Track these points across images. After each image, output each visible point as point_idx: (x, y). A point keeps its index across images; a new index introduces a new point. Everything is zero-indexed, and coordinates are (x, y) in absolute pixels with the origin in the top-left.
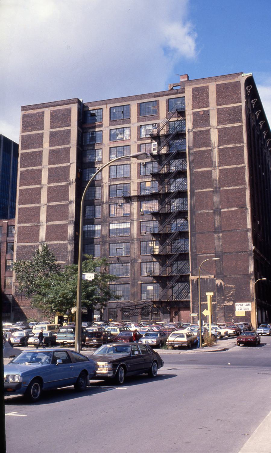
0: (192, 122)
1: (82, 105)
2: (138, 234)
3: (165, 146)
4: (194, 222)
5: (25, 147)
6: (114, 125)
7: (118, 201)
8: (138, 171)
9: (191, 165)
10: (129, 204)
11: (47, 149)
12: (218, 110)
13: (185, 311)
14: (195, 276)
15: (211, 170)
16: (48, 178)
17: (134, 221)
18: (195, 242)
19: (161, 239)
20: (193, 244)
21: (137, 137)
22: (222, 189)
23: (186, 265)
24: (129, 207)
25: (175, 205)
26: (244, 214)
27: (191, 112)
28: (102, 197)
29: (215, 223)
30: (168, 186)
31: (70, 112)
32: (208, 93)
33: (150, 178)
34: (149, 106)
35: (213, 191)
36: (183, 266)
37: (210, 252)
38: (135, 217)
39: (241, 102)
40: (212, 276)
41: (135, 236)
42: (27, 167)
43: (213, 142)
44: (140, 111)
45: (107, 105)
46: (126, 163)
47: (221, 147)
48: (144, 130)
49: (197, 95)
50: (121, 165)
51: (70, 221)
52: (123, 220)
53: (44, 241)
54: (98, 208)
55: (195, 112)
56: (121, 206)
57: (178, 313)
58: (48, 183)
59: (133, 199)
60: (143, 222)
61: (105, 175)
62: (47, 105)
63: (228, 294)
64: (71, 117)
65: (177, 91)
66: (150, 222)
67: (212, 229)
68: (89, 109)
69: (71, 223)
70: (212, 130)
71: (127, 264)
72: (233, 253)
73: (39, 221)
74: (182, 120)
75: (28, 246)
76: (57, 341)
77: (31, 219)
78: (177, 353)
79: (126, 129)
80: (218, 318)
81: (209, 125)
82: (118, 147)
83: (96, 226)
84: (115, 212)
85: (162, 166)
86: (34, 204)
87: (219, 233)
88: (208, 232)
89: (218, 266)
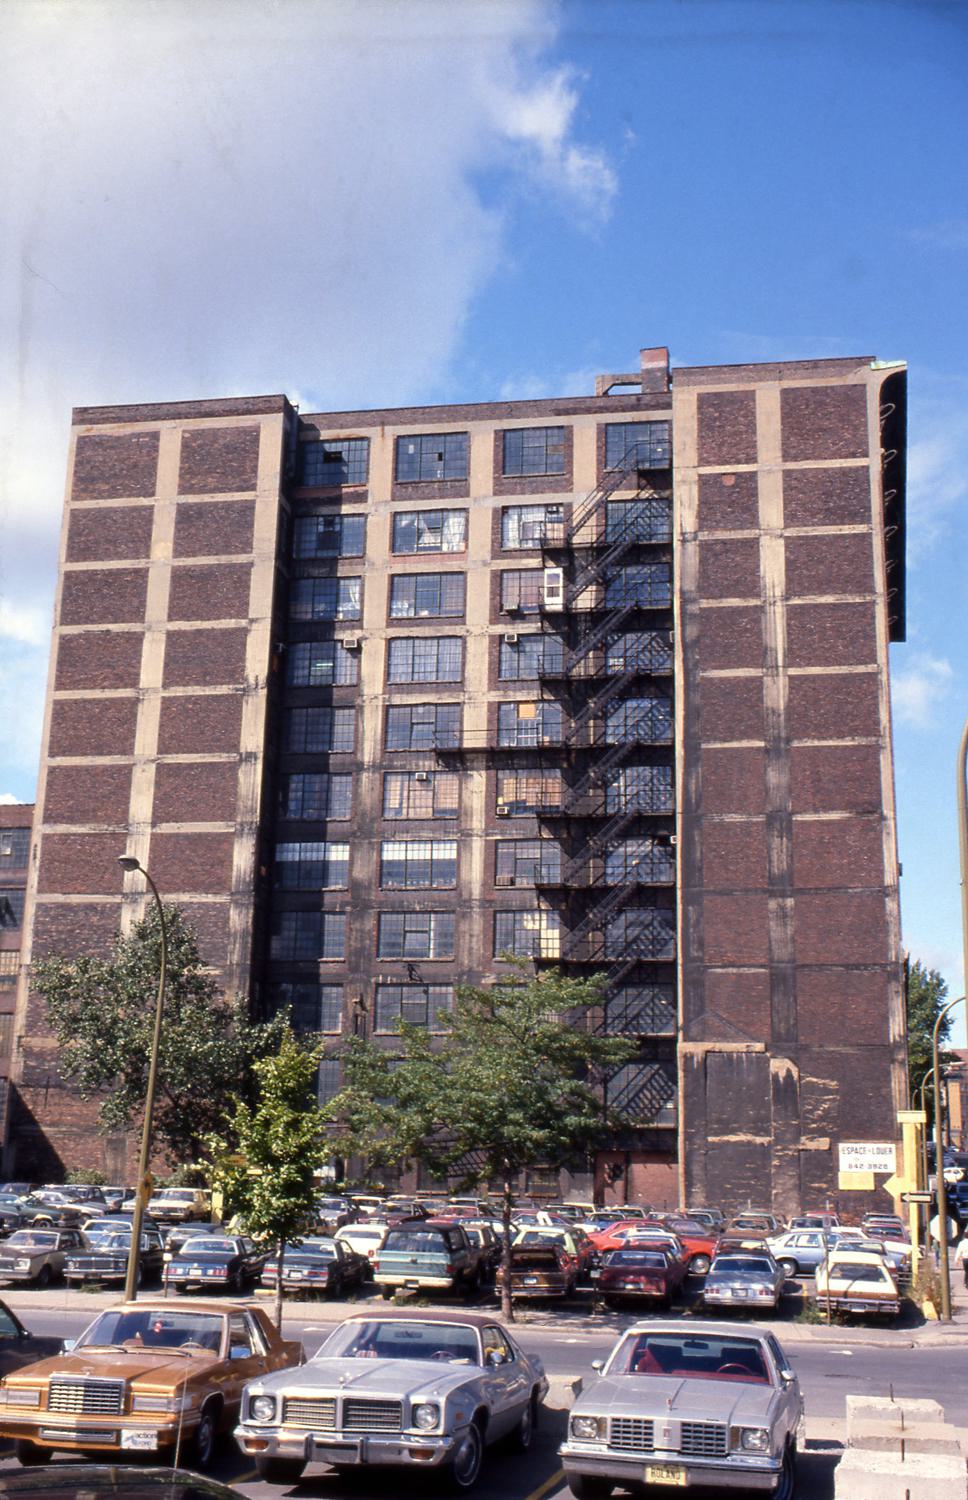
0: (696, 508)
1: (295, 421)
2: (484, 884)
3: (591, 584)
4: (698, 855)
5: (83, 550)
6: (411, 499)
7: (417, 765)
8: (490, 664)
9: (690, 655)
10: (455, 778)
11: (165, 565)
12: (787, 474)
13: (648, 1165)
14: (700, 1044)
15: (762, 677)
16: (166, 665)
17: (471, 835)
18: (698, 922)
19: (567, 906)
20: (691, 930)
21: (493, 546)
22: (796, 744)
23: (657, 1001)
24: (456, 787)
25: (622, 789)
26: (872, 835)
27: (693, 475)
28: (360, 747)
29: (770, 862)
30: (599, 722)
31: (256, 440)
32: (753, 414)
33: (532, 689)
34: (534, 442)
35: (766, 751)
36: (647, 1004)
37: (752, 961)
38: (477, 823)
39: (865, 455)
40: (759, 1046)
41: (476, 892)
42: (86, 623)
43: (767, 581)
44: (504, 457)
45: (386, 428)
46: (451, 634)
47: (796, 601)
48: (516, 525)
49: (716, 419)
50: (432, 638)
51: (242, 824)
52: (433, 831)
53: (139, 890)
54: (340, 784)
55: (706, 475)
56: (427, 780)
57: (621, 1172)
58: (165, 686)
59: (472, 761)
60: (505, 844)
61: (372, 668)
62: (172, 409)
63: (811, 1112)
64: (257, 459)
65: (639, 400)
66: (531, 844)
67: (762, 883)
68: (319, 435)
69: (246, 831)
70: (764, 541)
71: (444, 989)
72: (835, 968)
73: (123, 817)
74: (654, 499)
75: (78, 905)
76: (377, 1278)
77: (94, 811)
78: (906, 1343)
79: (451, 514)
80: (776, 1194)
81: (754, 522)
82: (422, 574)
83: (333, 847)
84: (405, 801)
85: (581, 654)
86: (109, 757)
87: (784, 895)
88: (747, 891)
89: (778, 1012)
